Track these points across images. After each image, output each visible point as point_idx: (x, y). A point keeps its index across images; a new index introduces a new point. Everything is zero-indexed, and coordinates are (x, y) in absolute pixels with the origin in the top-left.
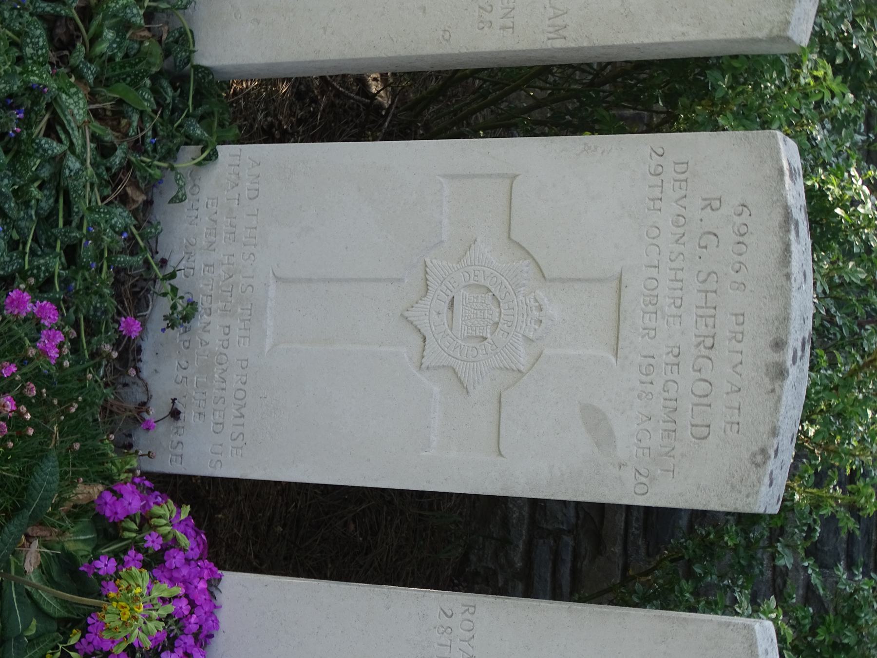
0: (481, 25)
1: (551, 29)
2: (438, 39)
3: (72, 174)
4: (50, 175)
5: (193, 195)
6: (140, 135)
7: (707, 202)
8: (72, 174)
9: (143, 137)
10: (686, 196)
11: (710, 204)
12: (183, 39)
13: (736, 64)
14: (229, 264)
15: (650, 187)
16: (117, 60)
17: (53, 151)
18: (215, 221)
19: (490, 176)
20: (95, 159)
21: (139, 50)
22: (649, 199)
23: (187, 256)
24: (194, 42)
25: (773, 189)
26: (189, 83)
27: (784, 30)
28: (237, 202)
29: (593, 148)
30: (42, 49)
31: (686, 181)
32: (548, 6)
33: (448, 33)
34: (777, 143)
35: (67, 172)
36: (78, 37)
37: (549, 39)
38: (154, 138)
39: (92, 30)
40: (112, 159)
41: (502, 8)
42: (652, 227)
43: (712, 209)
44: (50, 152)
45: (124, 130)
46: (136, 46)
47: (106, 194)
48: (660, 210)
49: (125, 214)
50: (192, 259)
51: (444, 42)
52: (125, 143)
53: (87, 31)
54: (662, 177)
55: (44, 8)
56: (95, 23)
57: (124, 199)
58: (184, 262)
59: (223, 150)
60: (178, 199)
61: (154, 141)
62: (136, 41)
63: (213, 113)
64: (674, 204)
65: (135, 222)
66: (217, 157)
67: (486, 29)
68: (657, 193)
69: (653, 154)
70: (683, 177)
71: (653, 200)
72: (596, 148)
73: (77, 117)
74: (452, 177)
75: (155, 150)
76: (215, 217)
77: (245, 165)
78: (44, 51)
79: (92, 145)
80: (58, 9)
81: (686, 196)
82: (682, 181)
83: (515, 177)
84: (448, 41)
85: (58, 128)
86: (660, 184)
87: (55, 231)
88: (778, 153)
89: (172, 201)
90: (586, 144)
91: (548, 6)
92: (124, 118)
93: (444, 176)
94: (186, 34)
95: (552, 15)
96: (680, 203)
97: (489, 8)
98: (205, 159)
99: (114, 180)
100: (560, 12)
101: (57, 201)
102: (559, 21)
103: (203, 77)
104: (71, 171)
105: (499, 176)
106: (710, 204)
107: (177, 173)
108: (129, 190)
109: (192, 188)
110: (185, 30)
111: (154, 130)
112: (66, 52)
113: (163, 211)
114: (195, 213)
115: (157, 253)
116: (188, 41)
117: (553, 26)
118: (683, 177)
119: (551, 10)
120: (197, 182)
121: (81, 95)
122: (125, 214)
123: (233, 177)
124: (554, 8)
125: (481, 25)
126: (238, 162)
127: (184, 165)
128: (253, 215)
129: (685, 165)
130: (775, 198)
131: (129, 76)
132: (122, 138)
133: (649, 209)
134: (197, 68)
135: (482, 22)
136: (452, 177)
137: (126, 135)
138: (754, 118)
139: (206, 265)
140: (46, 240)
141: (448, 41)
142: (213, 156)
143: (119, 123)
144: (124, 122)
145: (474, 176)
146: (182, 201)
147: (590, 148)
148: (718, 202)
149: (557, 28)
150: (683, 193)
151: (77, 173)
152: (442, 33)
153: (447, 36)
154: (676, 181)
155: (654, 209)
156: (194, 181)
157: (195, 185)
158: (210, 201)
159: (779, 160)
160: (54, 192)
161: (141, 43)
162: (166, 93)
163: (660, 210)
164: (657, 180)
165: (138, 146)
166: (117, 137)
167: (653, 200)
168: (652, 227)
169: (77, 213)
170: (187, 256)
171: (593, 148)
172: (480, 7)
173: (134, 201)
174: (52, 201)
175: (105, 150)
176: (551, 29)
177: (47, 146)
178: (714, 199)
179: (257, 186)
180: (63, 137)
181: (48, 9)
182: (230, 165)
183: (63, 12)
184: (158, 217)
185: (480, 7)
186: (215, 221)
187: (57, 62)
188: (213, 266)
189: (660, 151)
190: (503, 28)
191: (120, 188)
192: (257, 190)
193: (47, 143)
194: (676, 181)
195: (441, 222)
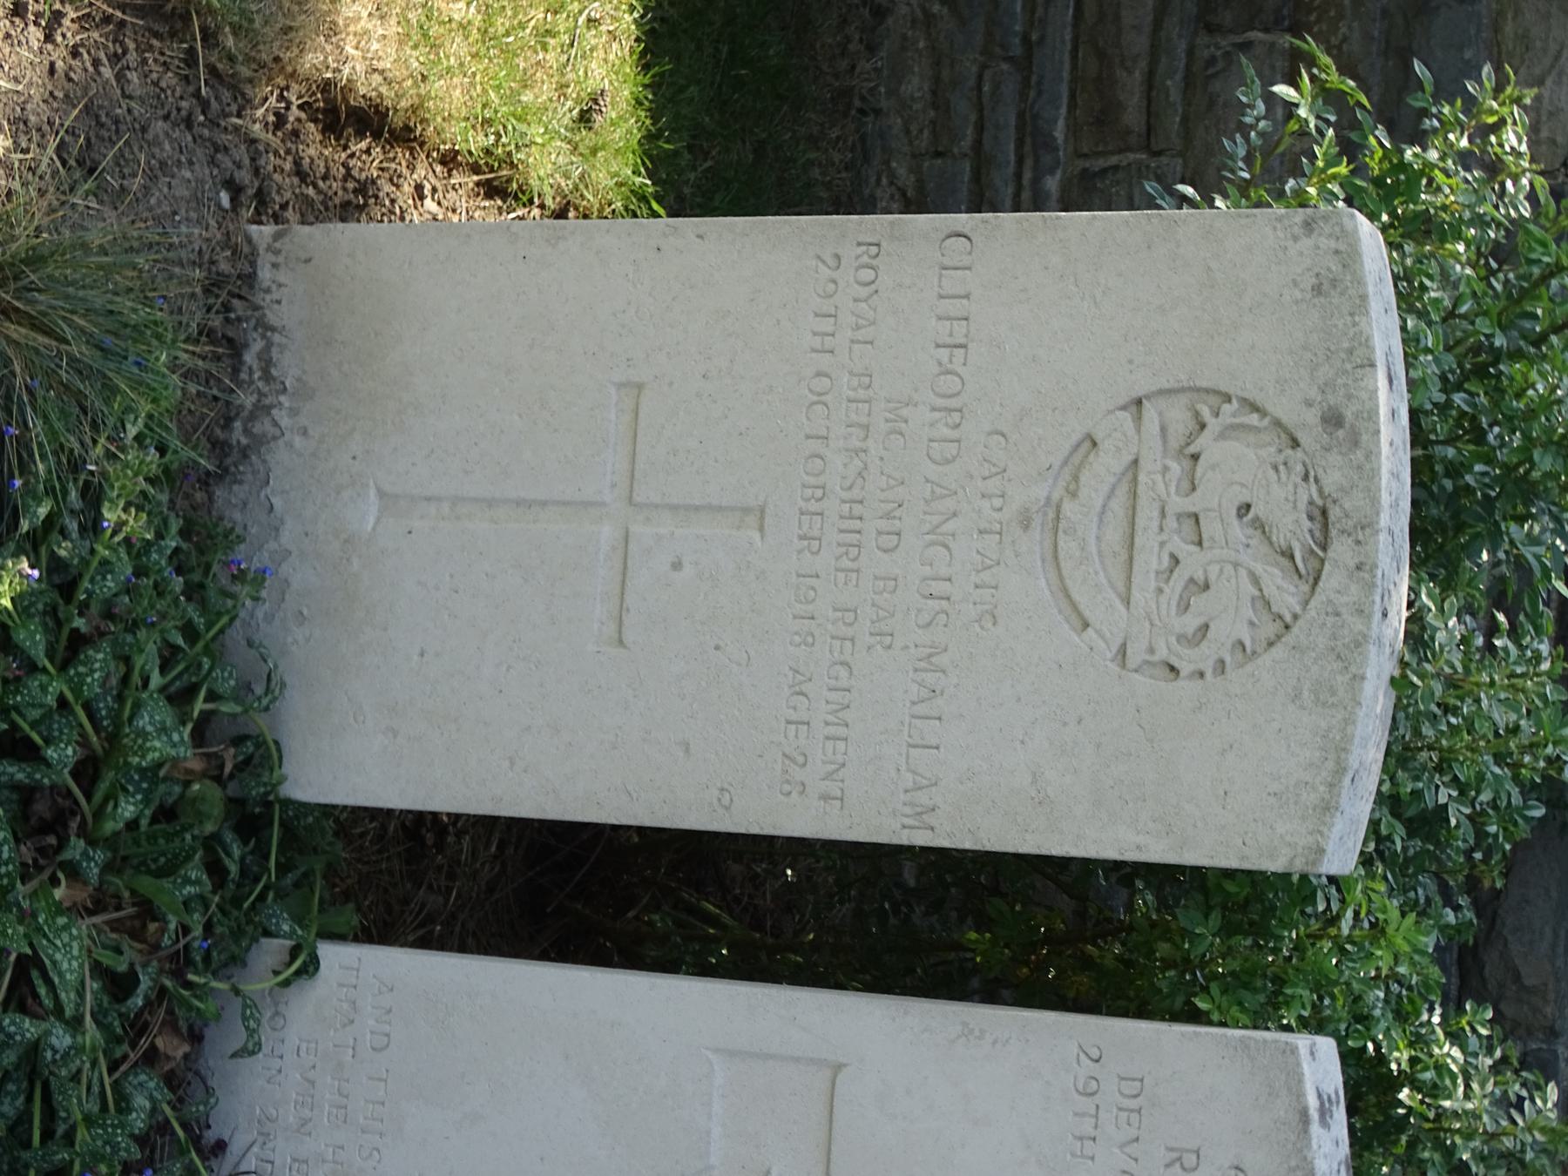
0: (787, 788)
1: (908, 810)
2: (710, 804)
3: (58, 1057)
4: (19, 1058)
5: (274, 1029)
6: (182, 942)
7: (1175, 1155)
8: (58, 1057)
9: (186, 947)
10: (1137, 1139)
11: (1180, 1159)
12: (260, 756)
13: (1231, 887)
14: (335, 1162)
15: (1076, 1114)
16: (143, 829)
17: (23, 1036)
18: (312, 1083)
19: (797, 1060)
20: (100, 1006)
21: (182, 796)
22: (1075, 1137)
23: (261, 1139)
24: (280, 758)
25: (1290, 1146)
26: (271, 824)
27: (1314, 863)
28: (350, 1052)
29: (977, 1033)
30: (6, 864)
31: (1139, 1111)
32: (903, 768)
33: (727, 796)
34: (1299, 1064)
35: (49, 1055)
36: (73, 813)
37: (904, 827)
38: (205, 939)
39: (98, 796)
40: (129, 1002)
41: (824, 762)
42: (989, 434)
43: (1184, 1169)
44: (18, 1038)
45: (152, 940)
46: (177, 789)
47: (118, 1054)
48: (1092, 1158)
49: (152, 1084)
50: (270, 1145)
51: (721, 811)
52: (155, 963)
53: (88, 797)
54: (1097, 1099)
55: (12, 775)
56: (103, 787)
57: (151, 1057)
58: (255, 1149)
59: (329, 953)
60: (250, 1050)
61: (205, 945)
62: (177, 782)
63: (313, 871)
64: (1117, 1151)
65: (170, 1096)
66: (317, 969)
67: (794, 794)
68: (1087, 1127)
69: (1082, 1056)
70: (1133, 1104)
71: (1081, 1139)
72: (982, 1032)
73: (68, 976)
74: (732, 1054)
75: (207, 958)
76: (311, 1075)
77: (368, 980)
78: (11, 867)
79: (95, 985)
80: (38, 776)
81: (1137, 1139)
82: (1132, 1111)
83: (838, 1068)
84: (727, 808)
85: (35, 974)
86: (1093, 1112)
87: (26, 1155)
88: (1301, 1081)
89: (234, 1055)
90: (965, 1024)
91: (903, 768)
92: (154, 919)
93: (717, 1051)
94: (268, 748)
95: (910, 785)
96: (1127, 1150)
97: (801, 759)
98: (298, 973)
99: (137, 1027)
100: (925, 782)
101: (29, 1099)
102: (923, 798)
103: (297, 817)
104: (55, 1051)
105: (812, 1061)
106: (1180, 1159)
107: (244, 997)
108: (159, 1042)
109: (272, 1018)
110: (265, 742)
111: (208, 928)
112: (52, 840)
113: (215, 1058)
114: (277, 1063)
115: (209, 1127)
116: (270, 756)
117: (912, 804)
118: (1133, 1104)
119: (909, 776)
120: (282, 1008)
121: (74, 932)
122: (152, 1084)
123: (345, 1006)
124: (914, 773)
125: (787, 788)
126: (354, 981)
127: (259, 986)
128: (380, 1080)
129: (1138, 1084)
130: (1293, 1163)
131: (164, 854)
132: (150, 953)
133: (1073, 1155)
134: (287, 803)
135: (788, 782)
136: (732, 1054)
137: (156, 947)
138: (1260, 999)
139: (294, 1160)
140: (9, 1164)
141: (727, 808)
142: (311, 967)
143: (144, 926)
144: (153, 927)
145: (770, 1057)
146: (253, 1053)
147: (972, 1031)
148: (1194, 1157)
149: (919, 810)
150: (1133, 1133)
151: (66, 1055)
152: (716, 793)
153: (726, 799)
154: (1120, 1109)
155: (1082, 1156)
156: (276, 1004)
157: (277, 1013)
158: (304, 1046)
159: (1300, 1095)
160: (25, 1085)
161: (187, 784)
162: (229, 855)
163: (1092, 1158)
164: (1088, 1105)
165: (180, 963)
166: (140, 951)
167: (1081, 1139)
168: (989, 434)
169: (65, 1120)
170: (261, 1139)
171: (977, 1033)
172: (784, 755)
173: (168, 1058)
174: (22, 1099)
175: (119, 985)
176: (908, 810)
177: (12, 1029)
178: (1188, 1151)
179: (387, 1028)
180: (42, 991)
181: (20, 776)
182: (341, 985)
183: (46, 781)
184: (211, 1063)
185: (784, 755)
186: (312, 1083)
187: (35, 860)
188: (306, 1162)
189: (1095, 1053)
190: (826, 798)
191: (144, 1043)
192: (388, 1035)
193: (13, 1023)
194: (1120, 1109)
195: (708, 1133)
